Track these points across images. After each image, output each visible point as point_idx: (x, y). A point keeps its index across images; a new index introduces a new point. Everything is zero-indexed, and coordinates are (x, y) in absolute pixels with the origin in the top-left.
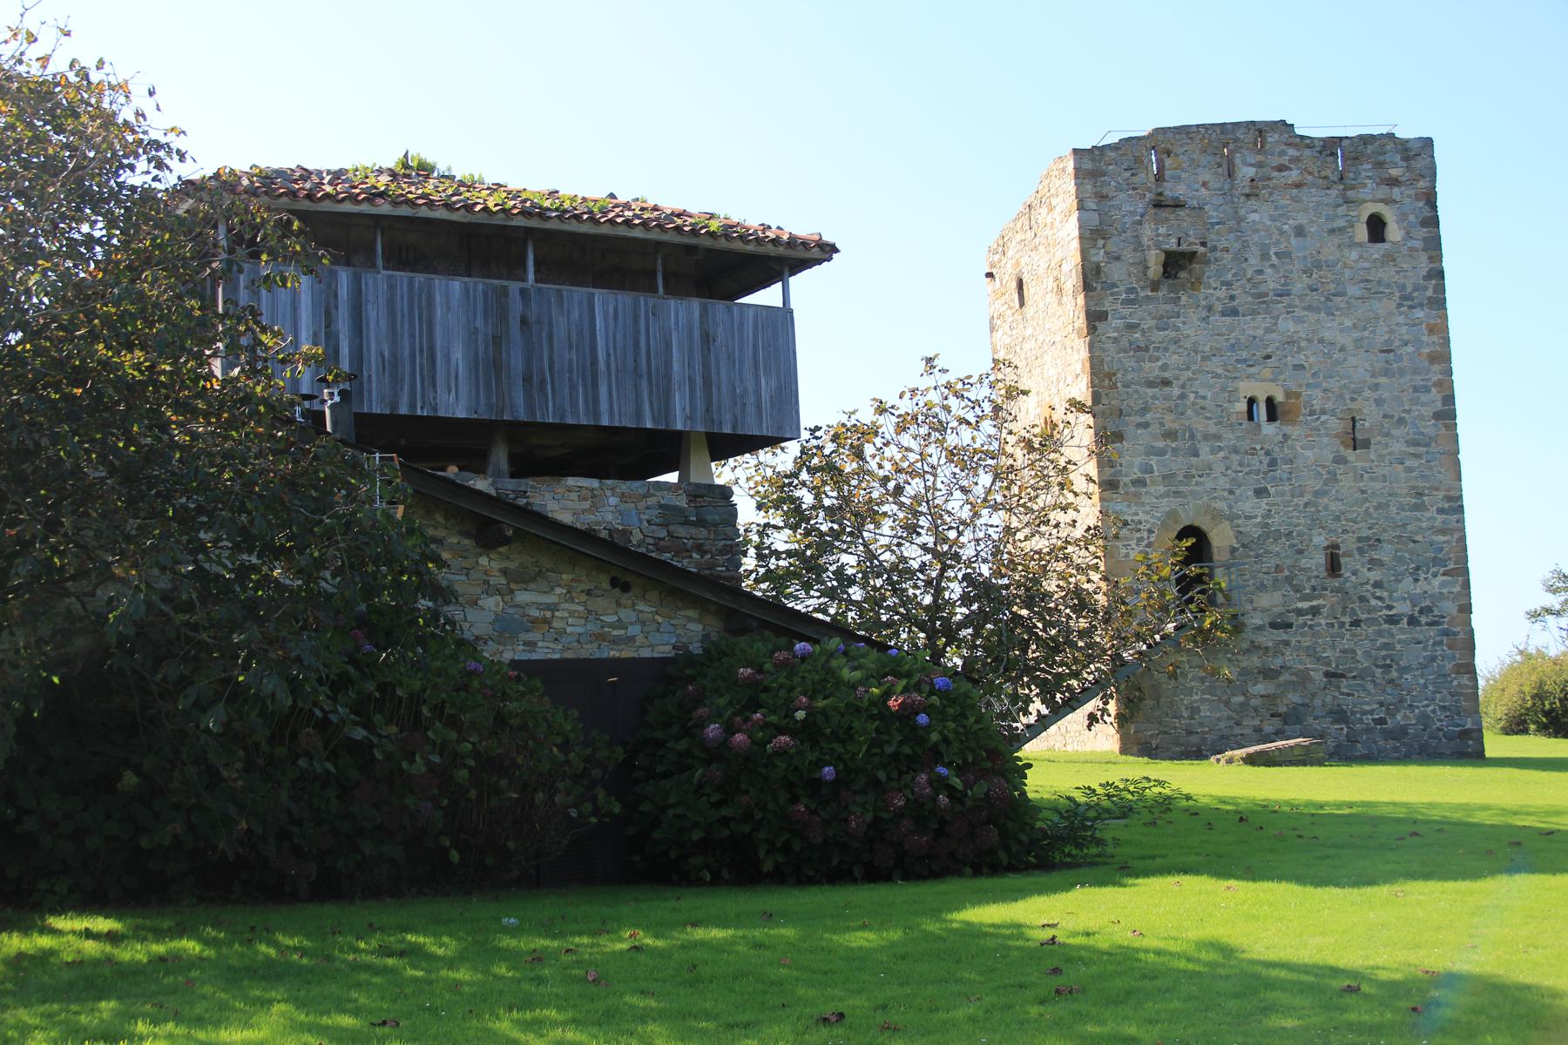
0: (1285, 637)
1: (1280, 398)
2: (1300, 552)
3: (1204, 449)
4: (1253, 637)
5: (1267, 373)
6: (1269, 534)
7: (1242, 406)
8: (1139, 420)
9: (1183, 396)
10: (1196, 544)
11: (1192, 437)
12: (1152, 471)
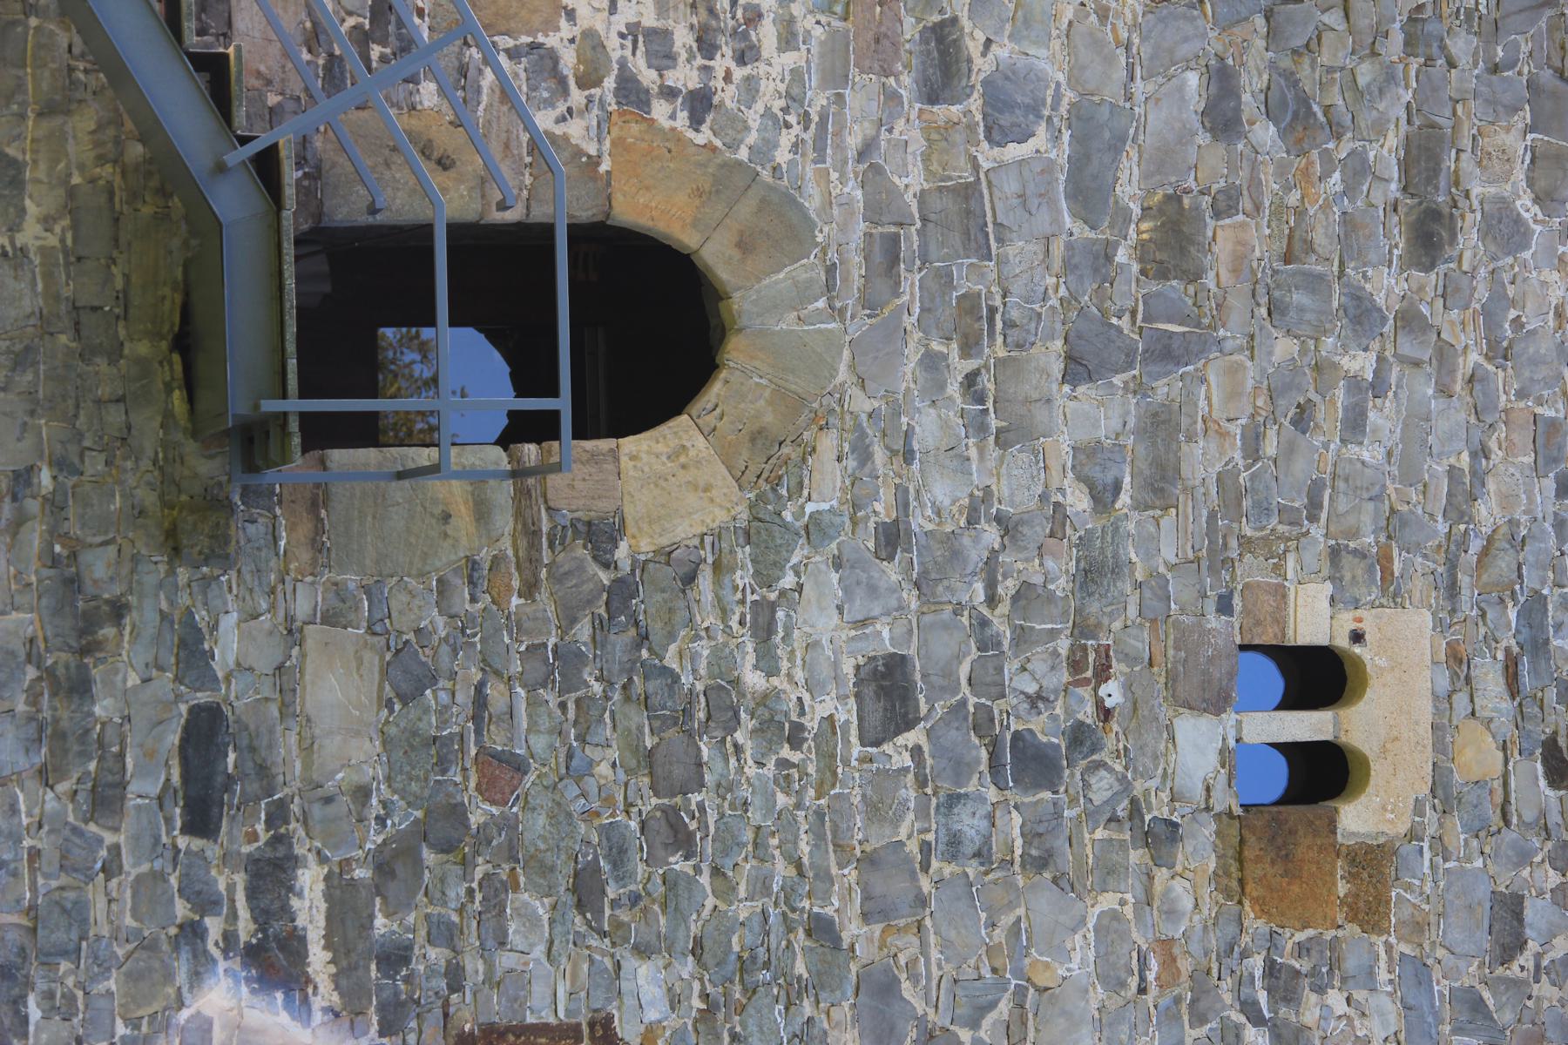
0: (142, 788)
1: (1356, 818)
2: (586, 891)
3: (1098, 413)
4: (145, 615)
5: (1478, 756)
6: (683, 725)
7: (1312, 620)
8: (1252, 85)
9: (1361, 315)
10: (624, 325)
11: (1166, 353)
12: (997, 134)
